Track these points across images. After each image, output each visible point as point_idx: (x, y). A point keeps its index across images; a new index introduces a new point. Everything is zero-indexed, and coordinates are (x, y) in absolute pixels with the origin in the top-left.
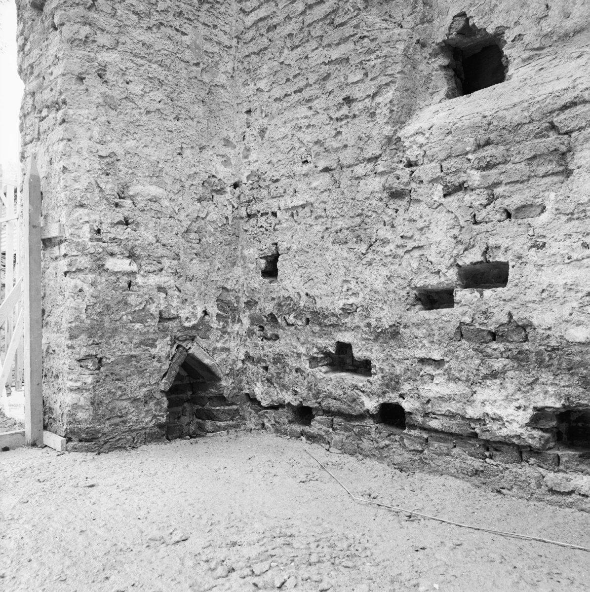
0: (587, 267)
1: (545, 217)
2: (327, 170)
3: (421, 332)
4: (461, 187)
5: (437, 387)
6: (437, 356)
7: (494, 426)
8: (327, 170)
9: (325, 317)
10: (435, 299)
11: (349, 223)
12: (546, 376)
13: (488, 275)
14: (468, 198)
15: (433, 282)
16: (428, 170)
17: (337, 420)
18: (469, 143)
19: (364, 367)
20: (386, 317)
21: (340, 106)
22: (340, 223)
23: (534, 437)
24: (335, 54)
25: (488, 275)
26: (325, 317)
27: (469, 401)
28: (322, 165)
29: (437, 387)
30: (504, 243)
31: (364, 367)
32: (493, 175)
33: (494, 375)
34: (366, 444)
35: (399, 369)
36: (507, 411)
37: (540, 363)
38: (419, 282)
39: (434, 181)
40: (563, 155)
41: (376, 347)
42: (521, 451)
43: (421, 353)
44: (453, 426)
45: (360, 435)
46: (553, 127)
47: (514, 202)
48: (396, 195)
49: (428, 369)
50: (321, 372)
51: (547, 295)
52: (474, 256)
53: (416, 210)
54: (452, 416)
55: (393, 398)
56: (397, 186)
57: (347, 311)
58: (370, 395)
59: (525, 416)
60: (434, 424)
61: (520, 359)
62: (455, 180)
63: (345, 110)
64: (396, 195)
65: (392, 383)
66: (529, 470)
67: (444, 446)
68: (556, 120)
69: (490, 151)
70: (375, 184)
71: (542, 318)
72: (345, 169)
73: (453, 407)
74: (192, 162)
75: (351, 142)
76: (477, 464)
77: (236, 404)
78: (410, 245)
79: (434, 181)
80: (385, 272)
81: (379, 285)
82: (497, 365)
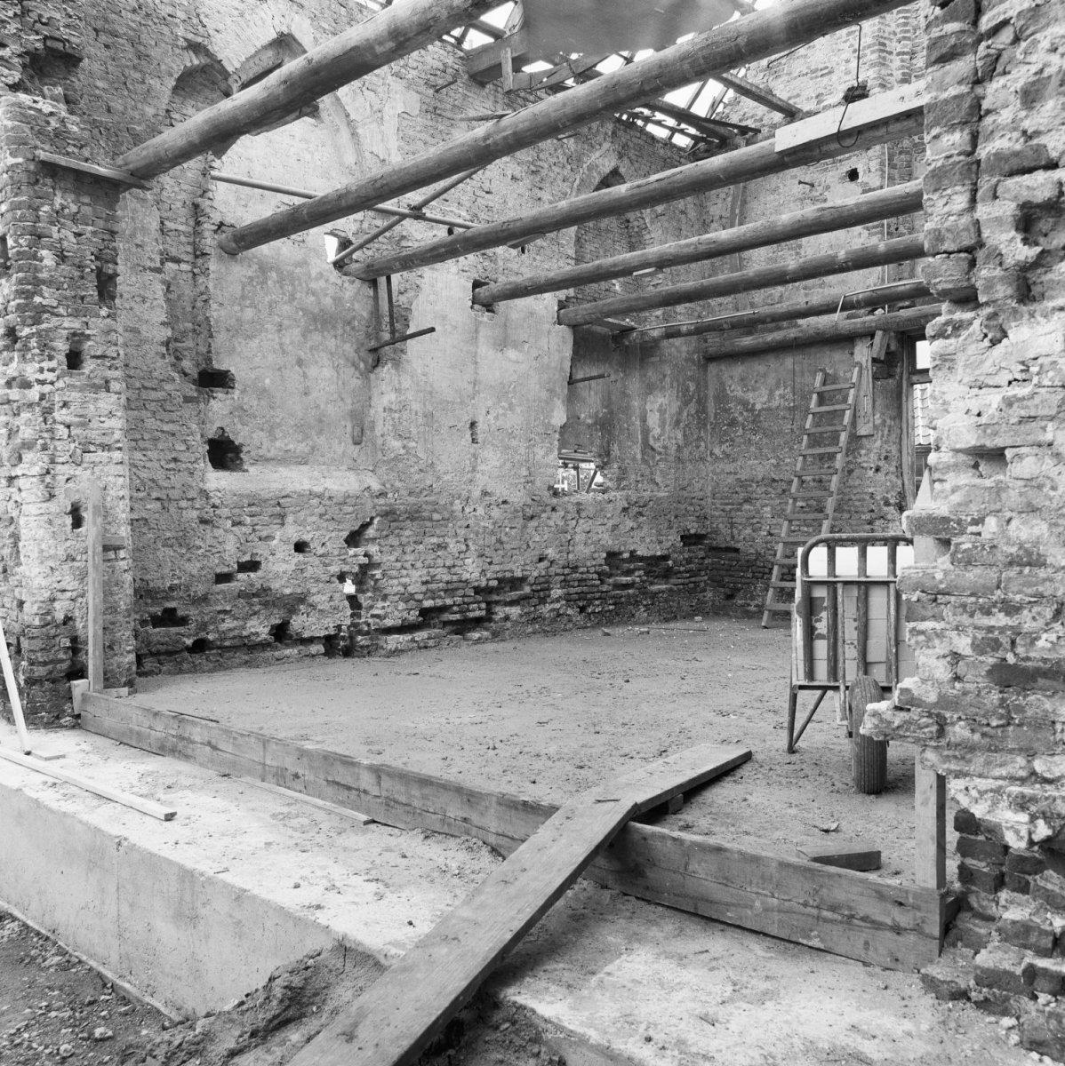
0: (1060, 309)
1: (275, 542)
2: (158, 499)
3: (220, 597)
4: (240, 523)
5: (229, 624)
6: (228, 608)
7: (253, 638)
8: (158, 499)
9: (157, 593)
10: (223, 578)
11: (175, 534)
12: (276, 611)
13: (252, 566)
14: (244, 529)
15: (226, 570)
16: (224, 512)
17: (162, 658)
18: (246, 501)
19: (183, 621)
20: (200, 589)
21: (168, 462)
22: (168, 534)
23: (271, 639)
24: (166, 428)
25: (252, 566)
26: (157, 593)
27: (243, 628)
28: (154, 495)
29: (229, 624)
30: (260, 552)
31: (183, 621)
32: (255, 519)
33: (255, 614)
34: (185, 666)
35: (206, 618)
36: (260, 629)
37: (274, 605)
38: (218, 571)
39: (227, 518)
40: (282, 517)
41: (192, 608)
42: (264, 646)
43: (219, 608)
44: (237, 642)
45: (181, 663)
46: (279, 504)
47: (264, 534)
48: (203, 521)
49: (221, 616)
50: (150, 629)
51: (277, 576)
52: (247, 558)
53: (218, 532)
54: (234, 637)
55: (202, 635)
56: (206, 517)
57: (172, 588)
58: (188, 637)
59: (267, 630)
60: (227, 643)
61: (266, 604)
62: (237, 519)
63: (172, 465)
64: (203, 521)
65: (203, 626)
66: (268, 654)
67: (231, 654)
68: (282, 501)
69: (254, 509)
70: (195, 514)
71: (275, 585)
72: (278, 373)
73: (236, 633)
74: (144, 976)
75: (178, 486)
76: (247, 658)
77: (120, 1014)
78: (214, 550)
79: (227, 518)
80: (198, 565)
81: (195, 572)
82: (256, 608)
